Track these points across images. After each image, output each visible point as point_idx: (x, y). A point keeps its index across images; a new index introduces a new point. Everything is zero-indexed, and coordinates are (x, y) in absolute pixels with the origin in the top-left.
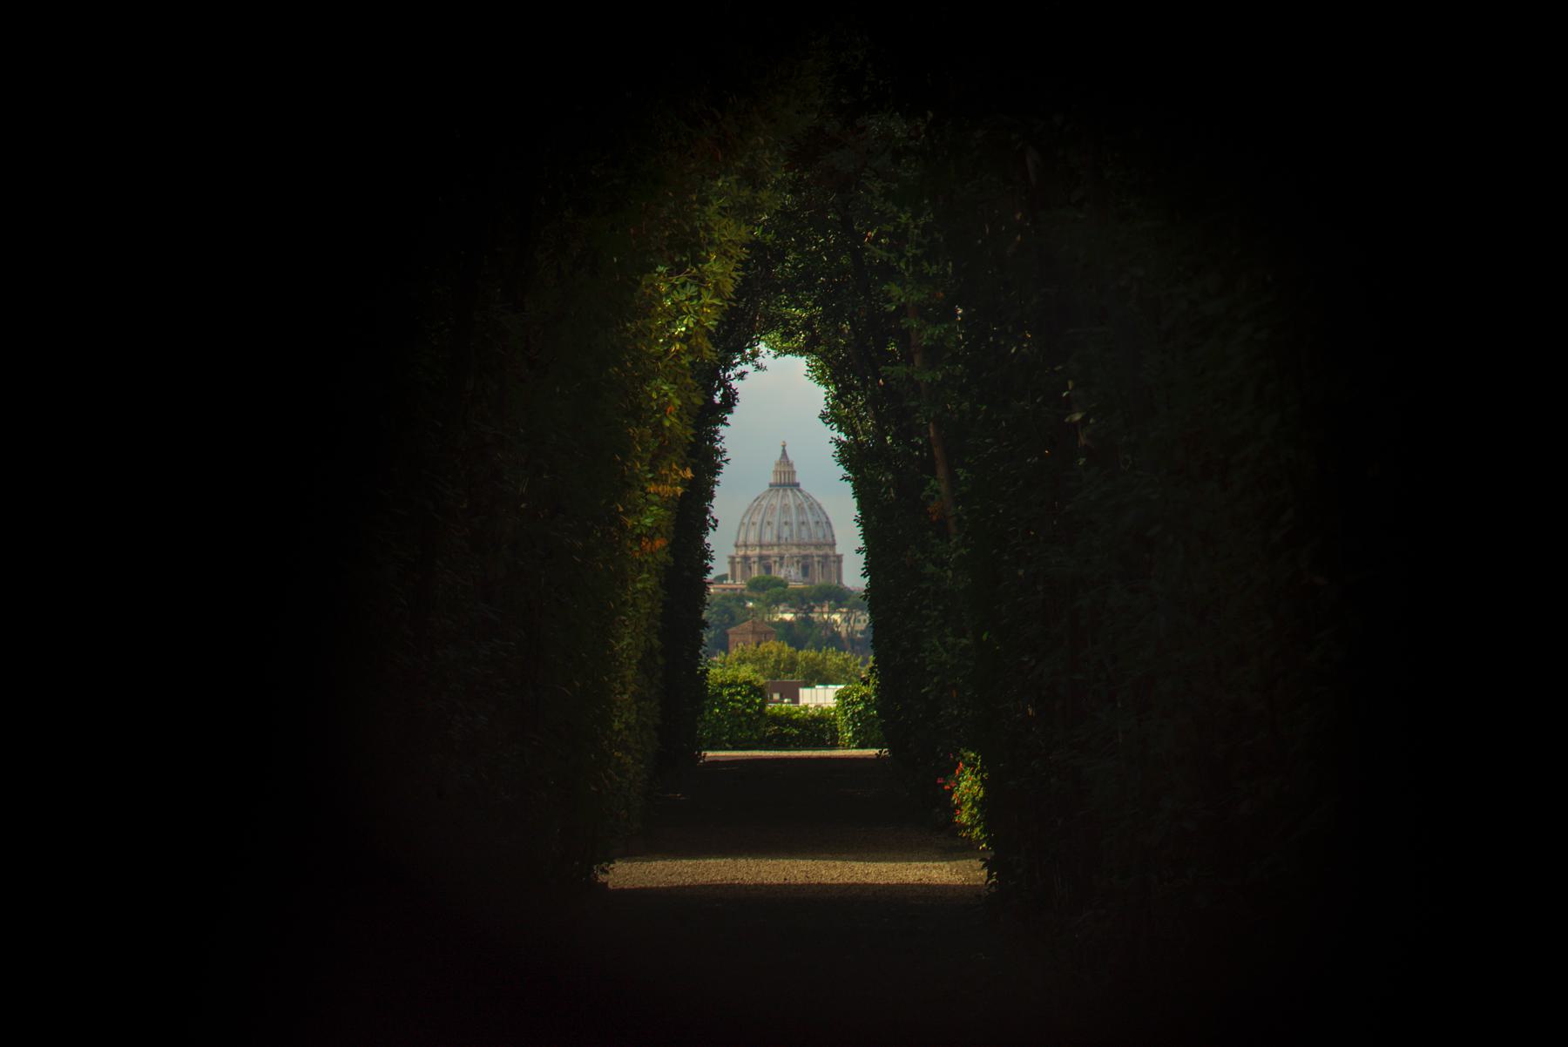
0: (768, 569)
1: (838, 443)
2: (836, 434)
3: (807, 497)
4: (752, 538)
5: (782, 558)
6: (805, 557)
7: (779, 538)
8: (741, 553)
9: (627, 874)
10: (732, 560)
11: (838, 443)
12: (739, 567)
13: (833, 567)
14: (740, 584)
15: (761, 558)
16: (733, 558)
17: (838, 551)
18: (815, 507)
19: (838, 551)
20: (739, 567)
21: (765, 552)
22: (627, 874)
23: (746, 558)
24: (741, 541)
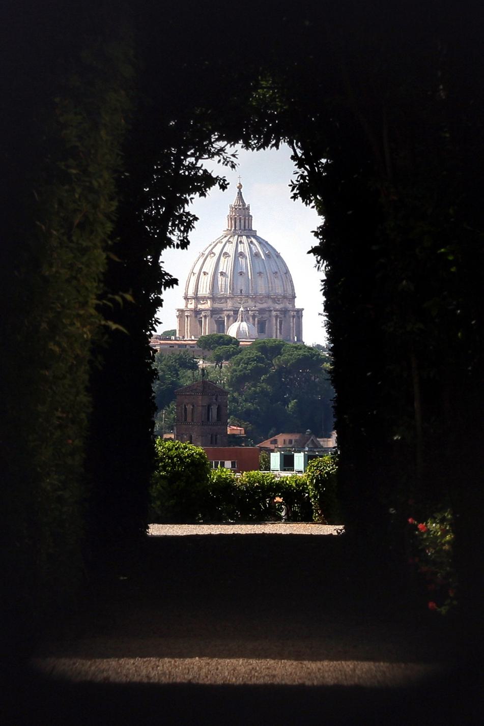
0: (221, 325)
1: (210, 189)
2: (269, 147)
3: (263, 243)
4: (204, 291)
5: (236, 312)
6: (261, 311)
7: (233, 289)
8: (191, 306)
9: (155, 530)
10: (181, 313)
11: (210, 189)
12: (187, 322)
13: (292, 323)
14: (190, 339)
15: (214, 312)
16: (181, 312)
17: (298, 305)
18: (273, 255)
19: (298, 305)
20: (187, 322)
21: (217, 305)
22: (155, 530)
23: (197, 312)
24: (191, 293)
